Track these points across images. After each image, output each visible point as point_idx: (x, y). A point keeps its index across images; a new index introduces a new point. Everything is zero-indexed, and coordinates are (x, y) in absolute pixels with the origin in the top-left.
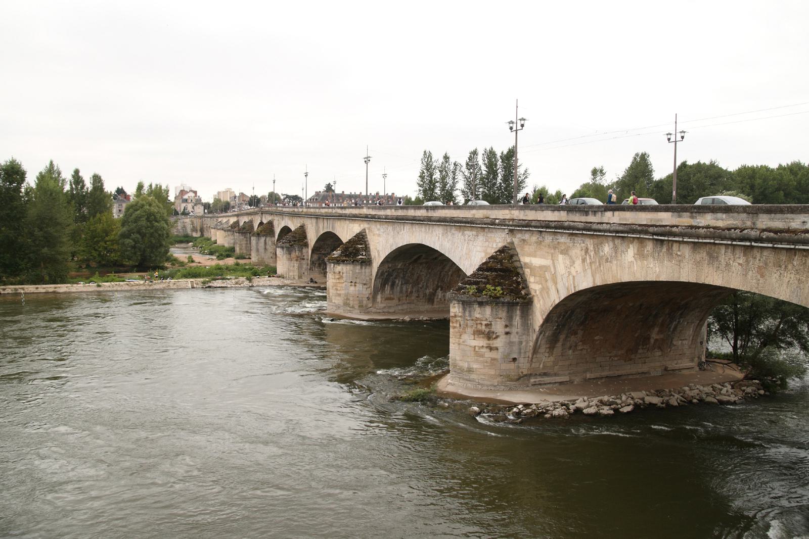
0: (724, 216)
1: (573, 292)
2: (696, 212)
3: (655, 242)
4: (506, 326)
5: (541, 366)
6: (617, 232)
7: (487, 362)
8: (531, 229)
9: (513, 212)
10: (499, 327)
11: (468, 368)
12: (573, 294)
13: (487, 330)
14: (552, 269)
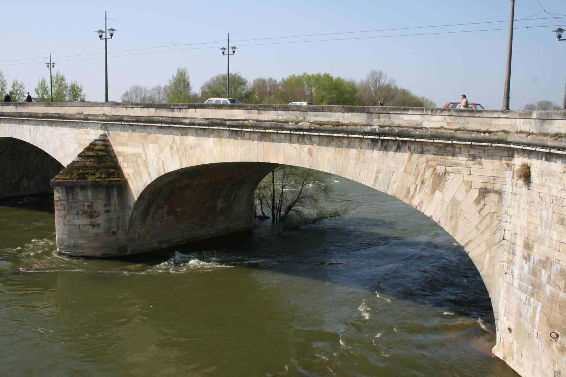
0: (283, 112)
1: (163, 174)
2: (262, 110)
3: (230, 132)
4: (106, 206)
5: (136, 236)
6: (199, 125)
7: (91, 237)
8: (123, 123)
9: (105, 109)
10: (99, 206)
11: (74, 244)
12: (163, 176)
13: (89, 210)
14: (143, 156)
